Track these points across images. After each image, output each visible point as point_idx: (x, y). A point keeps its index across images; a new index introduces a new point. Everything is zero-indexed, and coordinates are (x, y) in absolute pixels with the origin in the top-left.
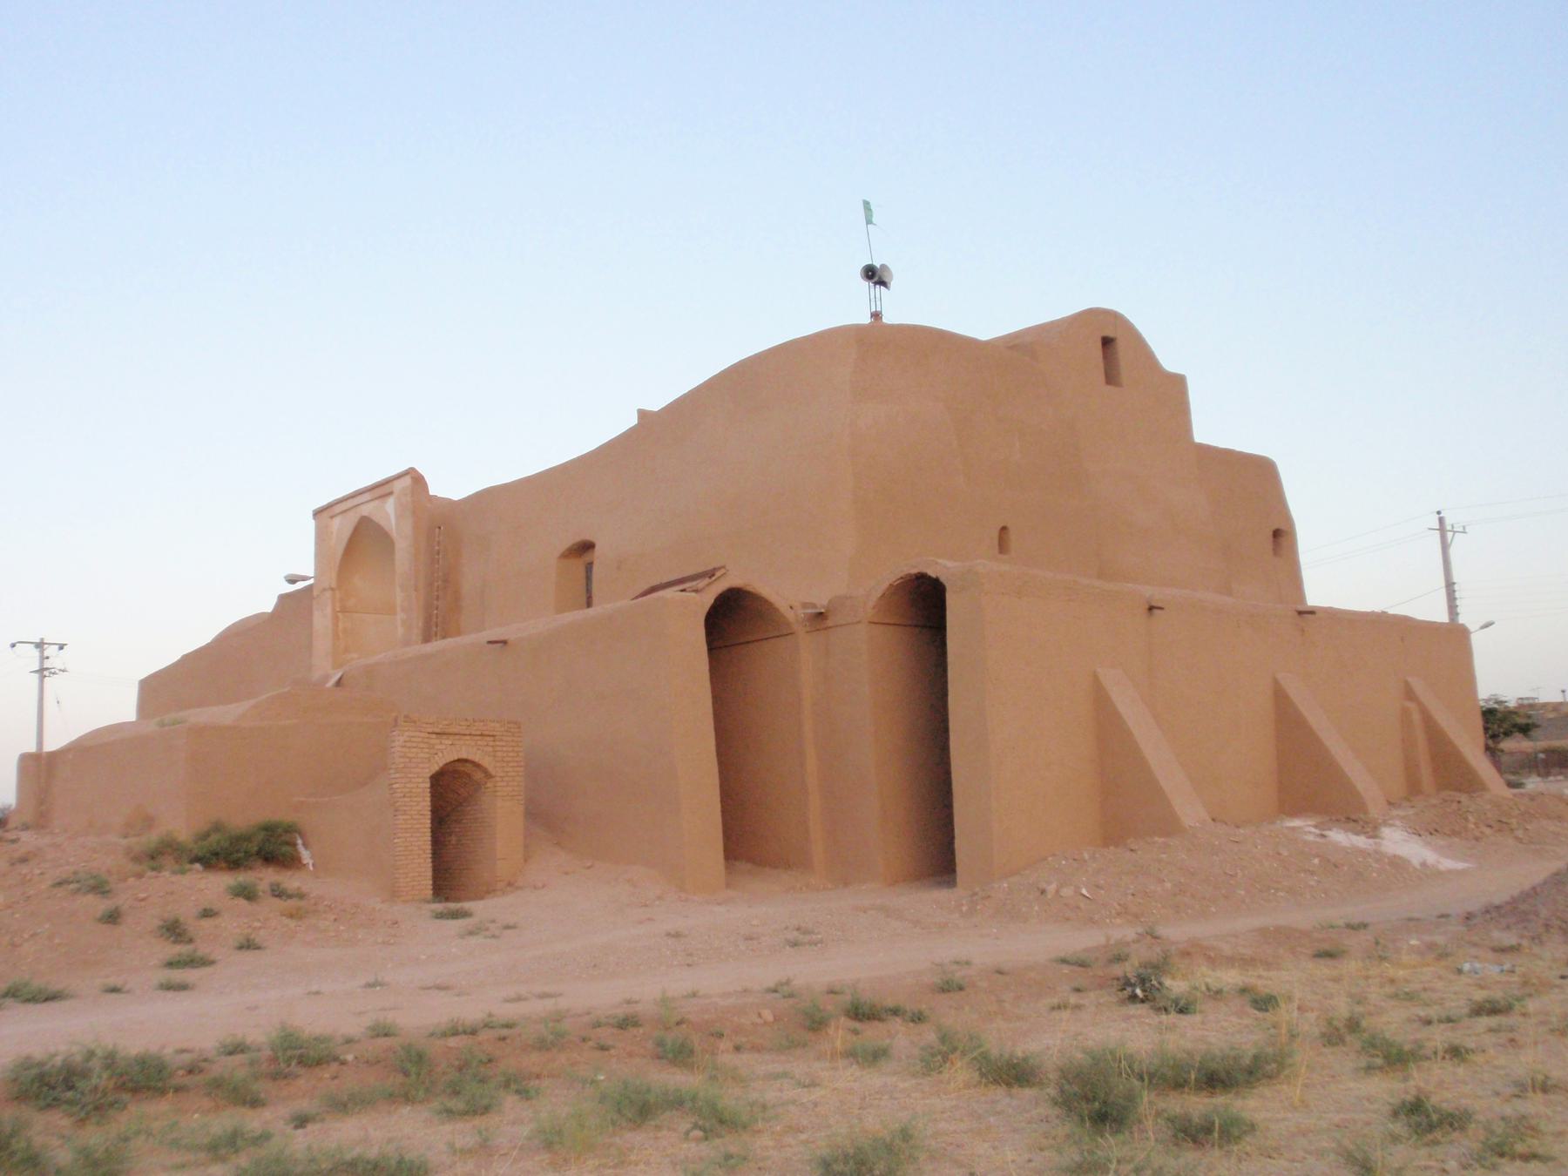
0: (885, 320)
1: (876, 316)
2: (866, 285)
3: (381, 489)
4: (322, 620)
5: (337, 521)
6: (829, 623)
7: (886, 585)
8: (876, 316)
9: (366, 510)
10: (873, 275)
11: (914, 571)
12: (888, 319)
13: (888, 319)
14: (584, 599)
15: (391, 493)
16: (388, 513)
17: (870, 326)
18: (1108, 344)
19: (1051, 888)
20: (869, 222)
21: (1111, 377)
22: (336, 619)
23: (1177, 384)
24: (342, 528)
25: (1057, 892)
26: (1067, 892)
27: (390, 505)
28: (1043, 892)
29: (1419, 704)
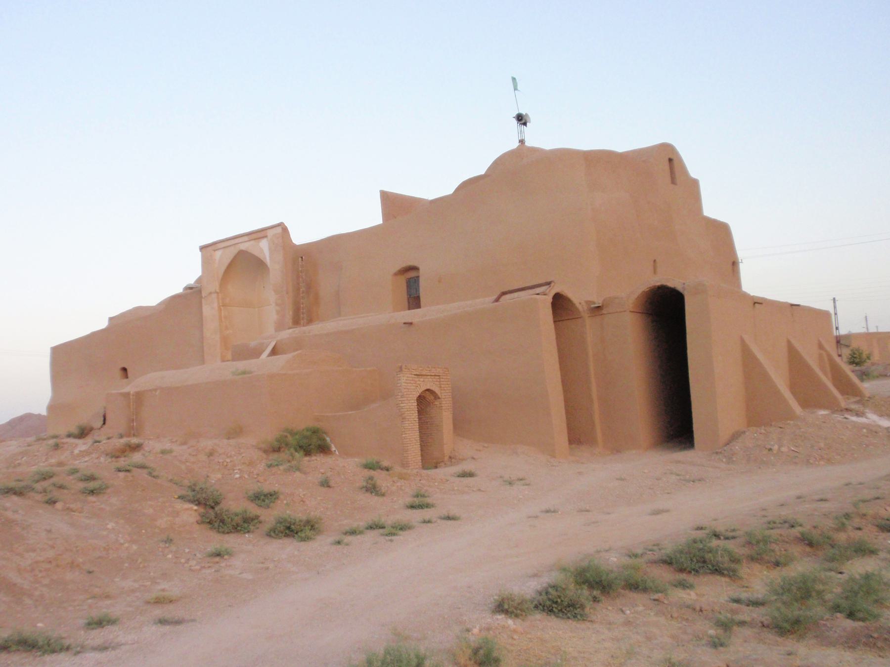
0: (526, 144)
1: (522, 142)
2: (515, 121)
3: (258, 235)
4: (209, 310)
5: (218, 254)
6: (604, 311)
7: (640, 291)
8: (522, 142)
9: (243, 247)
10: (521, 119)
11: (659, 284)
12: (528, 143)
13: (528, 143)
14: (837, 303)
15: (266, 237)
16: (263, 249)
17: (518, 149)
18: (668, 160)
19: (776, 447)
20: (516, 89)
21: (673, 181)
22: (220, 310)
23: (695, 183)
24: (222, 258)
25: (779, 449)
26: (784, 449)
27: (264, 245)
28: (770, 450)
29: (826, 351)
